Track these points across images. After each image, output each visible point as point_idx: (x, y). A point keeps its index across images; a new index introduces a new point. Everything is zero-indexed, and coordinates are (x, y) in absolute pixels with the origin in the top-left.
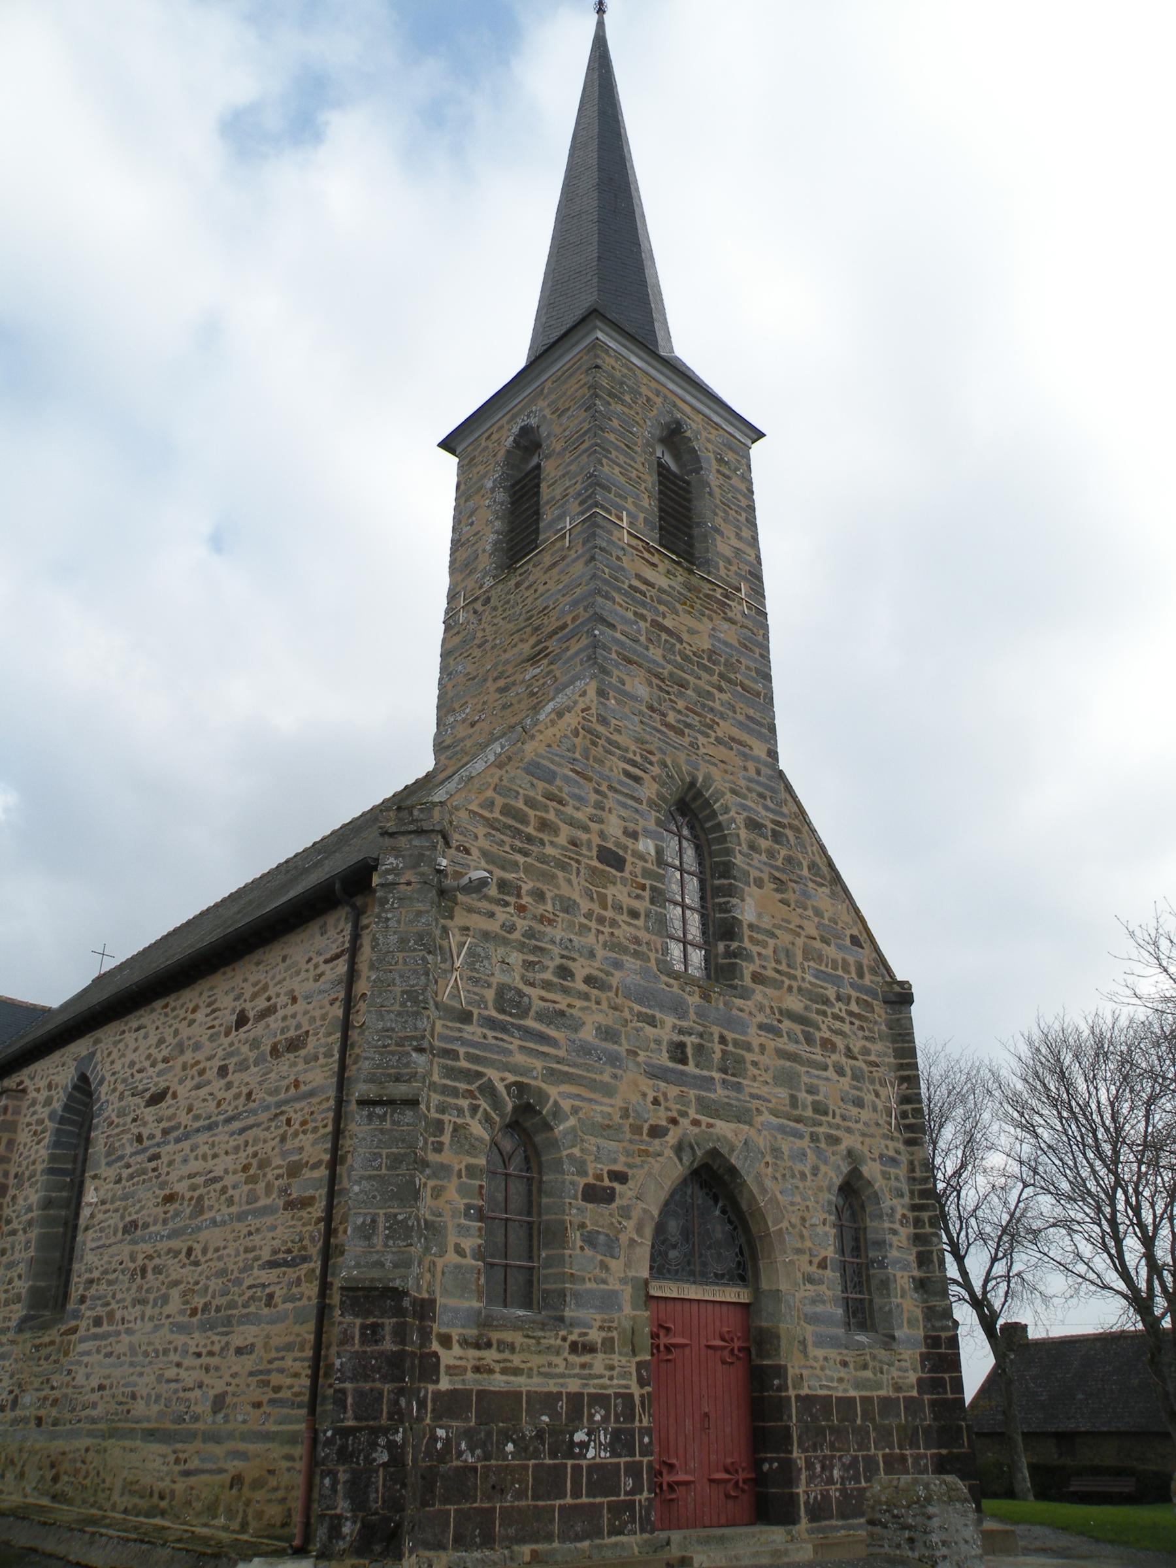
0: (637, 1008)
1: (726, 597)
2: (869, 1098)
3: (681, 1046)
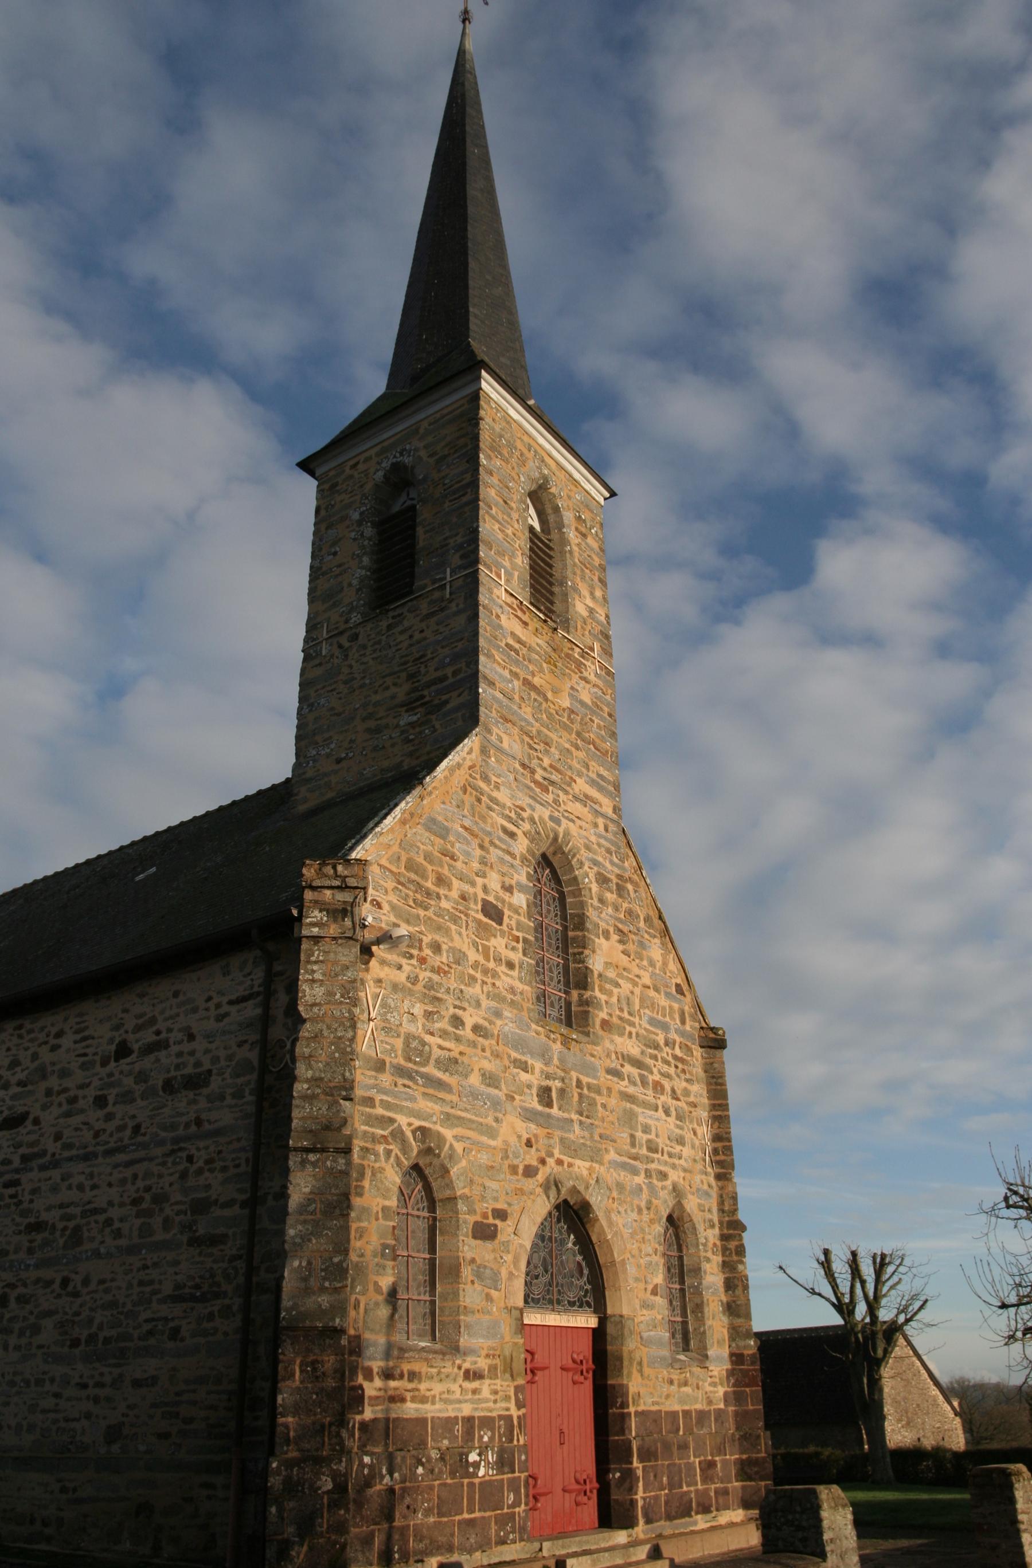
0: (514, 1055)
1: (583, 657)
2: (688, 1136)
3: (547, 1090)
